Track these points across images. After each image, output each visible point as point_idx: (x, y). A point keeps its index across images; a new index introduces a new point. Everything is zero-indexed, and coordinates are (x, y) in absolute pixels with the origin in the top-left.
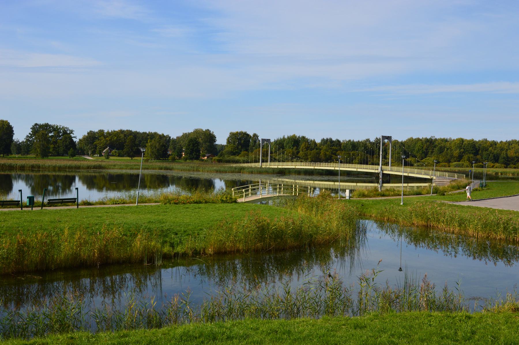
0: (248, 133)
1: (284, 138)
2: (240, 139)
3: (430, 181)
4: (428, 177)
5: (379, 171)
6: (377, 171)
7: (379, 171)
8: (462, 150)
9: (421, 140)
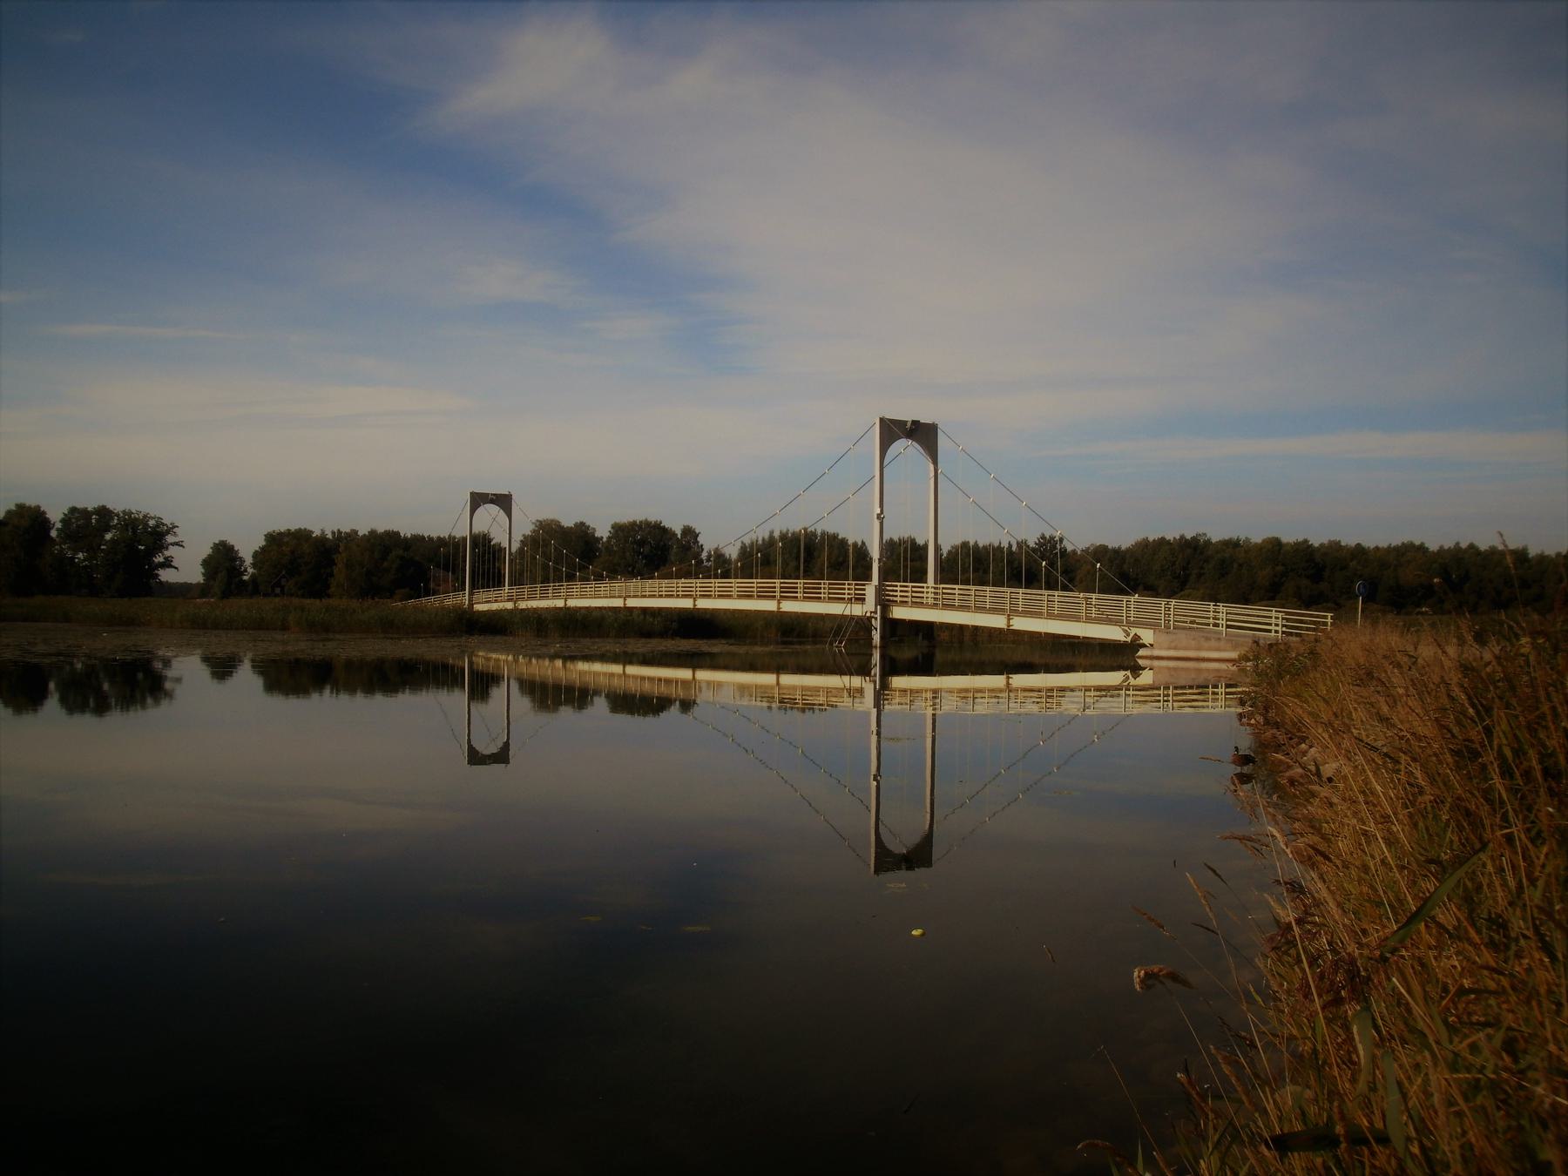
0: (666, 524)
1: (771, 537)
2: (642, 543)
3: (1121, 656)
4: (1114, 633)
5: (868, 607)
6: (857, 610)
7: (868, 607)
8: (1280, 568)
9: (1168, 542)
